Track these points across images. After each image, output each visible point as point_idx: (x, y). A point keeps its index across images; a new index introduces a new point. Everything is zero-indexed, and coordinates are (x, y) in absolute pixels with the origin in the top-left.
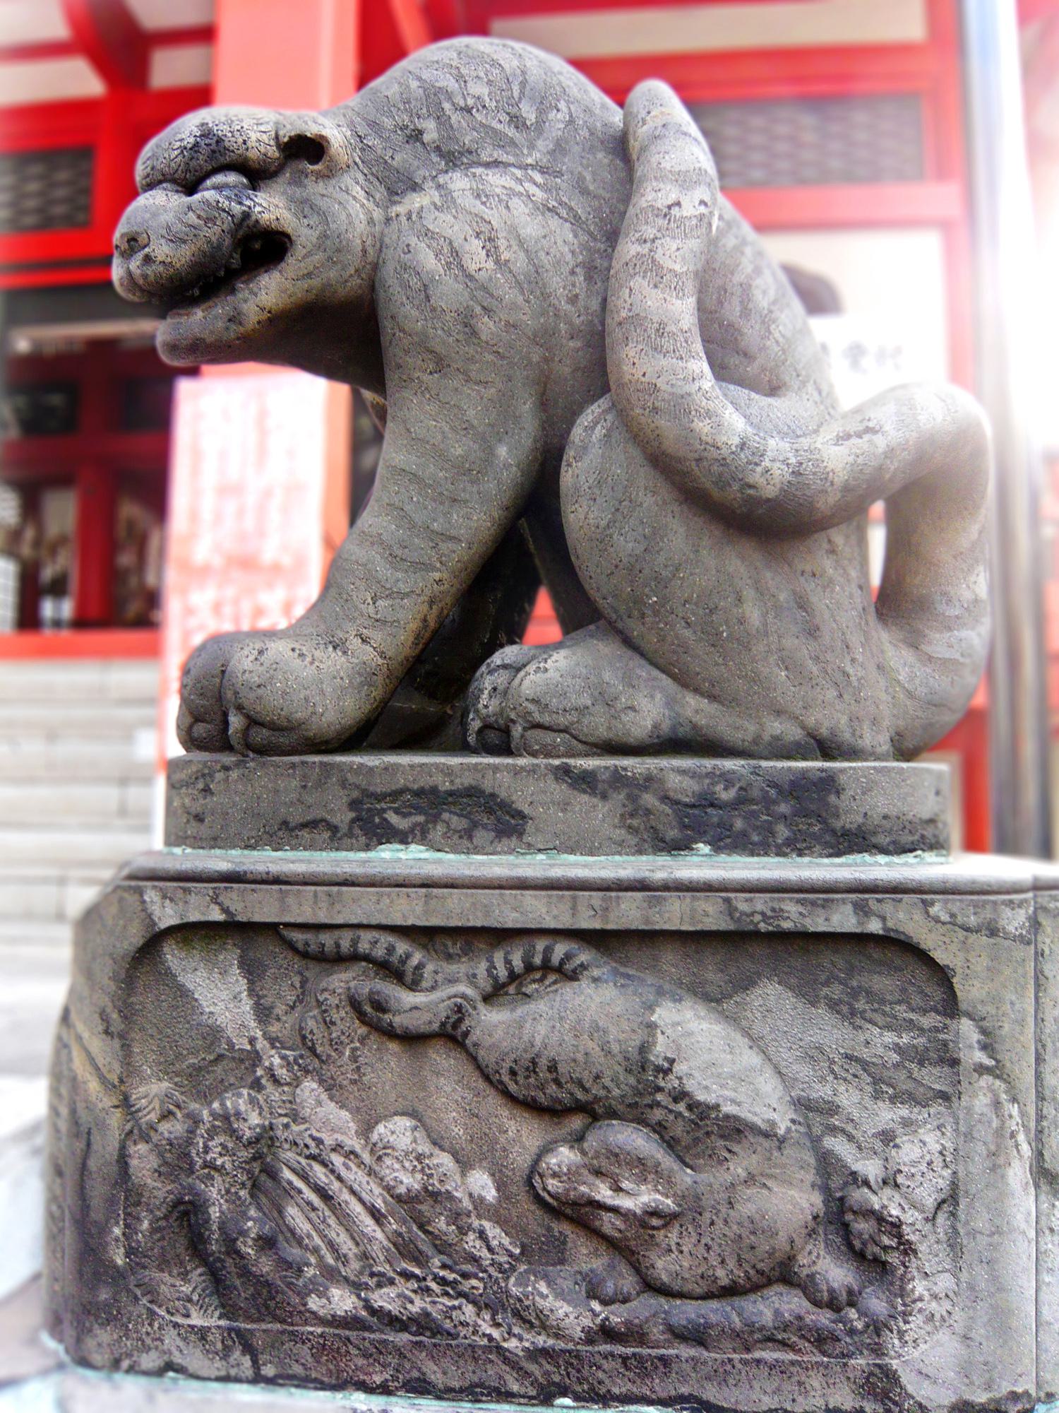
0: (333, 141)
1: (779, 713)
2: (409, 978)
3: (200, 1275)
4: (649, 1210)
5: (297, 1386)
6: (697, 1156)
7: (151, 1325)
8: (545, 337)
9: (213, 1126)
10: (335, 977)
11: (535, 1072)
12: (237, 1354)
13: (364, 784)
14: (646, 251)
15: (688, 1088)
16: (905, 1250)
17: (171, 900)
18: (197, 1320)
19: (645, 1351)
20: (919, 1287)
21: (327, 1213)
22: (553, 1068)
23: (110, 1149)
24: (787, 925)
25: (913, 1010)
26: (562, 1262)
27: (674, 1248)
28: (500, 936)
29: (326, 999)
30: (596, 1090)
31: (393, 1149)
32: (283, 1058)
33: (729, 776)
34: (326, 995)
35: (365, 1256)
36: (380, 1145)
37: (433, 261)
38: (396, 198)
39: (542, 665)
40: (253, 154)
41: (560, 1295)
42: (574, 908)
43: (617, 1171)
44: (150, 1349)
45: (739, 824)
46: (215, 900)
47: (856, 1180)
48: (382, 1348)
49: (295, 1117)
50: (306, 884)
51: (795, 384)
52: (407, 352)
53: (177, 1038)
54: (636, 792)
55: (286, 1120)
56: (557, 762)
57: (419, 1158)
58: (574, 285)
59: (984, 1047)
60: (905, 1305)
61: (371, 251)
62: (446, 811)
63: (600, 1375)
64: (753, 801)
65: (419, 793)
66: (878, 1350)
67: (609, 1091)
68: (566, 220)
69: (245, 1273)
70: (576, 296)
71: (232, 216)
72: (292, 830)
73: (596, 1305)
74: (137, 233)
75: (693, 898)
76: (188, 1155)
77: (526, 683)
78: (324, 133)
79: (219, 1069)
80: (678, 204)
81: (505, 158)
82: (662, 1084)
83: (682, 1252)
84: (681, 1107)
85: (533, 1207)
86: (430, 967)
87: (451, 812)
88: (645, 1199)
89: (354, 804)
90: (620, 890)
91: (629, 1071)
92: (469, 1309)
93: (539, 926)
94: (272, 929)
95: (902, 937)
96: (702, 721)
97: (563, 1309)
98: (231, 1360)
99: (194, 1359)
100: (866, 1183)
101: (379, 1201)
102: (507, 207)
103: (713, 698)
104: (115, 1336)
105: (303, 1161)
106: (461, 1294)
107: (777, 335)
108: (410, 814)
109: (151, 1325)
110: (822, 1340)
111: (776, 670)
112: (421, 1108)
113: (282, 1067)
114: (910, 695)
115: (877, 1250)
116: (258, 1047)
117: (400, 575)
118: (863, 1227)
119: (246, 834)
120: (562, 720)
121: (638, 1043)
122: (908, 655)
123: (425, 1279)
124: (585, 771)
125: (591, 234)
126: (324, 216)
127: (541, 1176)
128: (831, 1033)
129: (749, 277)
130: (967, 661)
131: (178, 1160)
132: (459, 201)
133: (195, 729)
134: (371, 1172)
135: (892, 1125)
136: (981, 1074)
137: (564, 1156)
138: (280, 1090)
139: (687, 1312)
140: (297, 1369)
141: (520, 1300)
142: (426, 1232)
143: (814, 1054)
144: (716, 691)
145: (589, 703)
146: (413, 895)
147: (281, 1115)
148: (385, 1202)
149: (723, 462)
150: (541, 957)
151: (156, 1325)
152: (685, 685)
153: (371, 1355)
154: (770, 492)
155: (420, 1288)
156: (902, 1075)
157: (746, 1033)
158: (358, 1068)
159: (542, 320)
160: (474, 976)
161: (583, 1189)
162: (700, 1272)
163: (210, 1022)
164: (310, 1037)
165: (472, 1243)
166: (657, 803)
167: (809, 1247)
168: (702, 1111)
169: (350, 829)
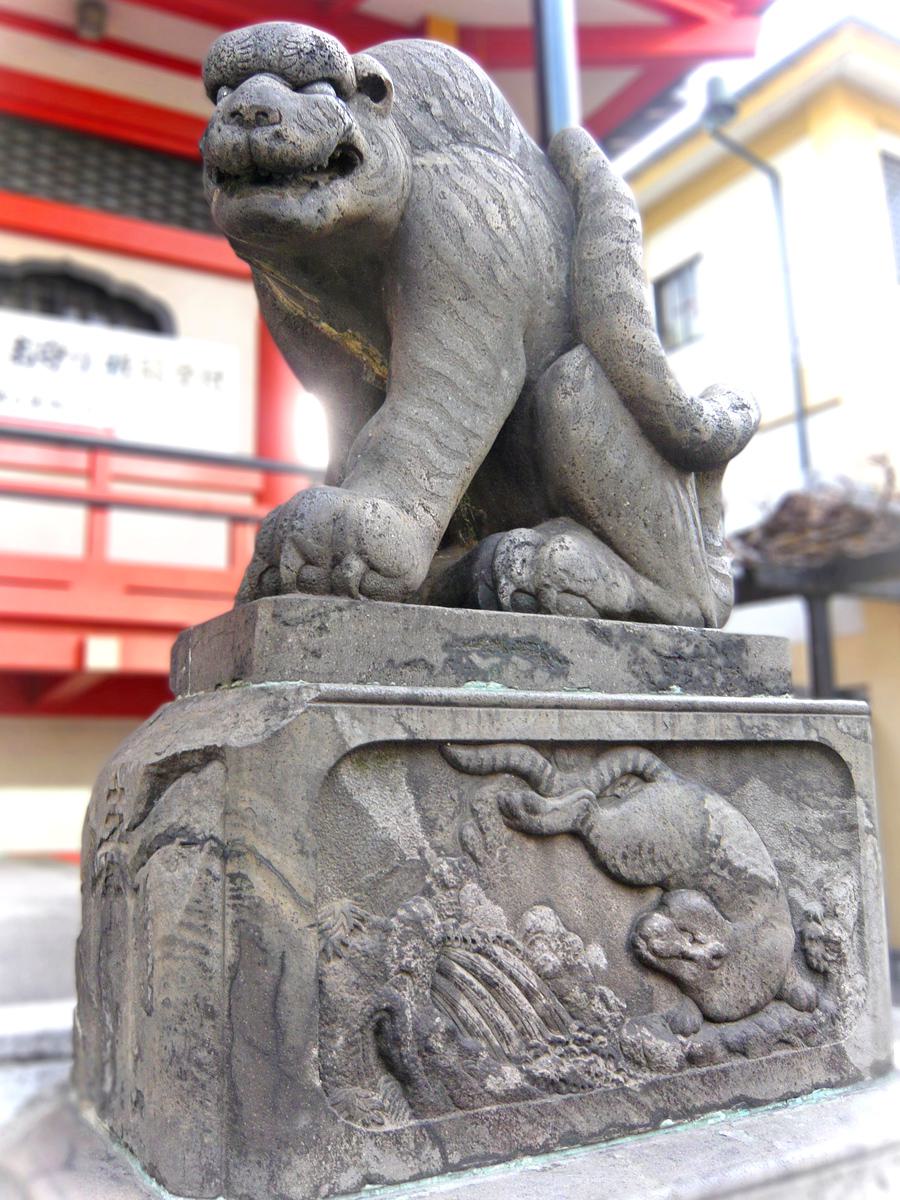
1: (690, 596)
2: (543, 787)
4: (715, 953)
5: (477, 1167)
6: (733, 910)
7: (349, 1141)
9: (406, 932)
10: (485, 788)
11: (640, 854)
14: (624, 248)
17: (359, 721)
18: (389, 1127)
19: (714, 1068)
20: (846, 987)
21: (493, 1000)
22: (651, 851)
23: (307, 970)
24: (771, 736)
26: (651, 1010)
28: (601, 748)
30: (676, 866)
31: (542, 932)
32: (451, 864)
35: (522, 1033)
36: (533, 931)
41: (658, 1035)
42: (654, 724)
43: (695, 926)
45: (696, 672)
46: (398, 720)
47: (809, 917)
48: (542, 1111)
49: (460, 917)
50: (470, 705)
52: (441, 277)
53: (355, 854)
60: (842, 1000)
65: (495, 640)
69: (433, 1069)
73: (682, 1038)
74: (270, 110)
76: (382, 963)
79: (393, 881)
82: (715, 856)
83: (729, 984)
84: (725, 873)
85: (631, 968)
86: (557, 775)
88: (710, 945)
89: (446, 647)
90: (680, 710)
92: (601, 1061)
93: (632, 739)
94: (439, 747)
95: (827, 743)
97: (665, 1045)
98: (423, 1157)
99: (390, 1165)
100: (816, 919)
101: (533, 981)
103: (657, 582)
104: (315, 1162)
105: (472, 956)
106: (595, 1051)
109: (349, 1141)
110: (807, 1034)
112: (552, 897)
113: (449, 872)
115: (826, 964)
118: (816, 949)
119: (358, 670)
120: (584, 588)
123: (567, 1043)
124: (604, 628)
128: (788, 814)
131: (374, 970)
133: (304, 571)
134: (525, 957)
137: (659, 921)
138: (447, 893)
139: (733, 1032)
140: (479, 1150)
141: (634, 1045)
143: (781, 830)
147: (449, 916)
148: (537, 980)
149: (682, 410)
151: (354, 1140)
152: (638, 571)
154: (706, 437)
156: (823, 840)
161: (677, 943)
163: (384, 836)
165: (597, 1006)
166: (649, 654)
169: (444, 669)
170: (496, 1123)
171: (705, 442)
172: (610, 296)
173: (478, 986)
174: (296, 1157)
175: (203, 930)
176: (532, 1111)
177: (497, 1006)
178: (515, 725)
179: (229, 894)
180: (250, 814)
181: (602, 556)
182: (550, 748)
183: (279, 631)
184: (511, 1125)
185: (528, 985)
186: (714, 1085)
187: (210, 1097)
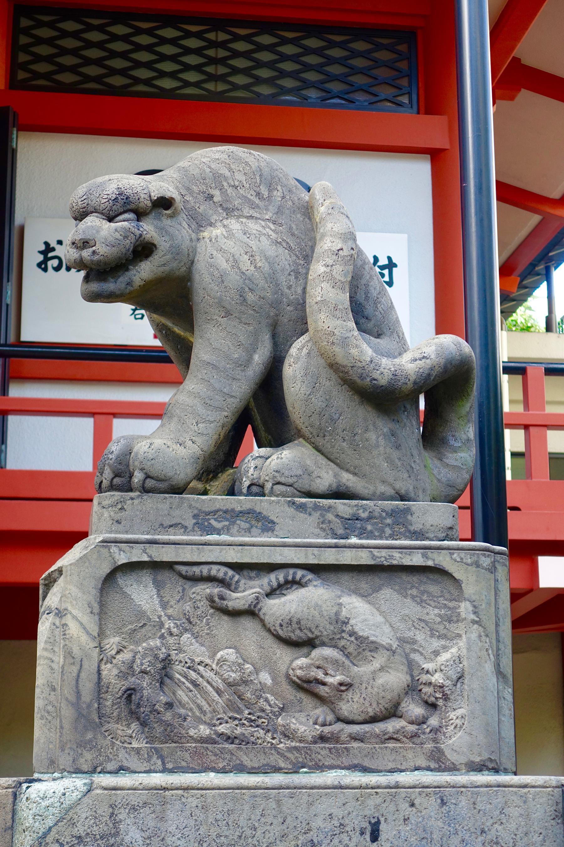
0: (176, 200)
2: (233, 587)
3: (135, 725)
6: (359, 660)
8: (276, 304)
11: (291, 624)
12: (155, 758)
13: (200, 508)
15: (356, 630)
16: (445, 698)
17: (124, 551)
18: (135, 745)
21: (196, 692)
22: (299, 622)
24: (395, 562)
25: (446, 600)
27: (350, 700)
29: (195, 597)
33: (365, 507)
34: (194, 595)
37: (225, 264)
38: (202, 229)
39: (280, 456)
40: (141, 205)
44: (111, 760)
45: (369, 527)
46: (144, 551)
48: (222, 751)
49: (180, 650)
51: (388, 333)
54: (325, 513)
55: (176, 652)
56: (289, 499)
57: (239, 665)
58: (290, 281)
59: (475, 613)
61: (191, 254)
62: (239, 520)
63: (319, 757)
64: (375, 518)
65: (226, 512)
66: (435, 741)
67: (322, 633)
68: (286, 249)
70: (291, 286)
71: (136, 236)
72: (165, 528)
74: (90, 240)
75: (356, 551)
77: (273, 463)
78: (173, 196)
79: (143, 630)
80: (342, 249)
81: (255, 215)
82: (345, 629)
83: (353, 701)
84: (353, 639)
85: (288, 687)
87: (241, 520)
89: (195, 516)
90: (326, 547)
91: (331, 623)
94: (170, 566)
95: (442, 568)
96: (350, 484)
98: (152, 762)
101: (221, 686)
102: (259, 241)
103: (355, 474)
104: (94, 756)
105: (185, 669)
107: (381, 309)
108: (222, 521)
111: (383, 463)
114: (439, 480)
116: (162, 619)
117: (209, 413)
121: (334, 611)
122: (437, 462)
124: (302, 503)
125: (297, 256)
126: (172, 237)
127: (293, 670)
129: (368, 281)
130: (465, 467)
132: (236, 235)
133: (115, 480)
135: (438, 648)
136: (474, 624)
140: (184, 764)
141: (284, 726)
142: (242, 699)
144: (356, 471)
145: (302, 474)
146: (236, 549)
147: (174, 650)
148: (223, 686)
150: (291, 576)
151: (115, 748)
152: (342, 468)
153: (218, 755)
154: (383, 381)
155: (239, 723)
156: (442, 627)
157: (378, 609)
158: (210, 628)
159: (276, 296)
160: (262, 585)
162: (361, 710)
163: (139, 609)
164: (188, 614)
166: (334, 518)
167: (406, 699)
168: (361, 640)
169: (193, 528)
170: (194, 753)
171: (382, 386)
172: (317, 303)
173: (188, 684)
174: (85, 752)
175: (52, 651)
176: (216, 750)
177: (198, 696)
179: (62, 634)
180: (69, 595)
182: (238, 567)
183: (101, 511)
184: (203, 754)
185: (218, 688)
186: (339, 755)
187: (52, 726)
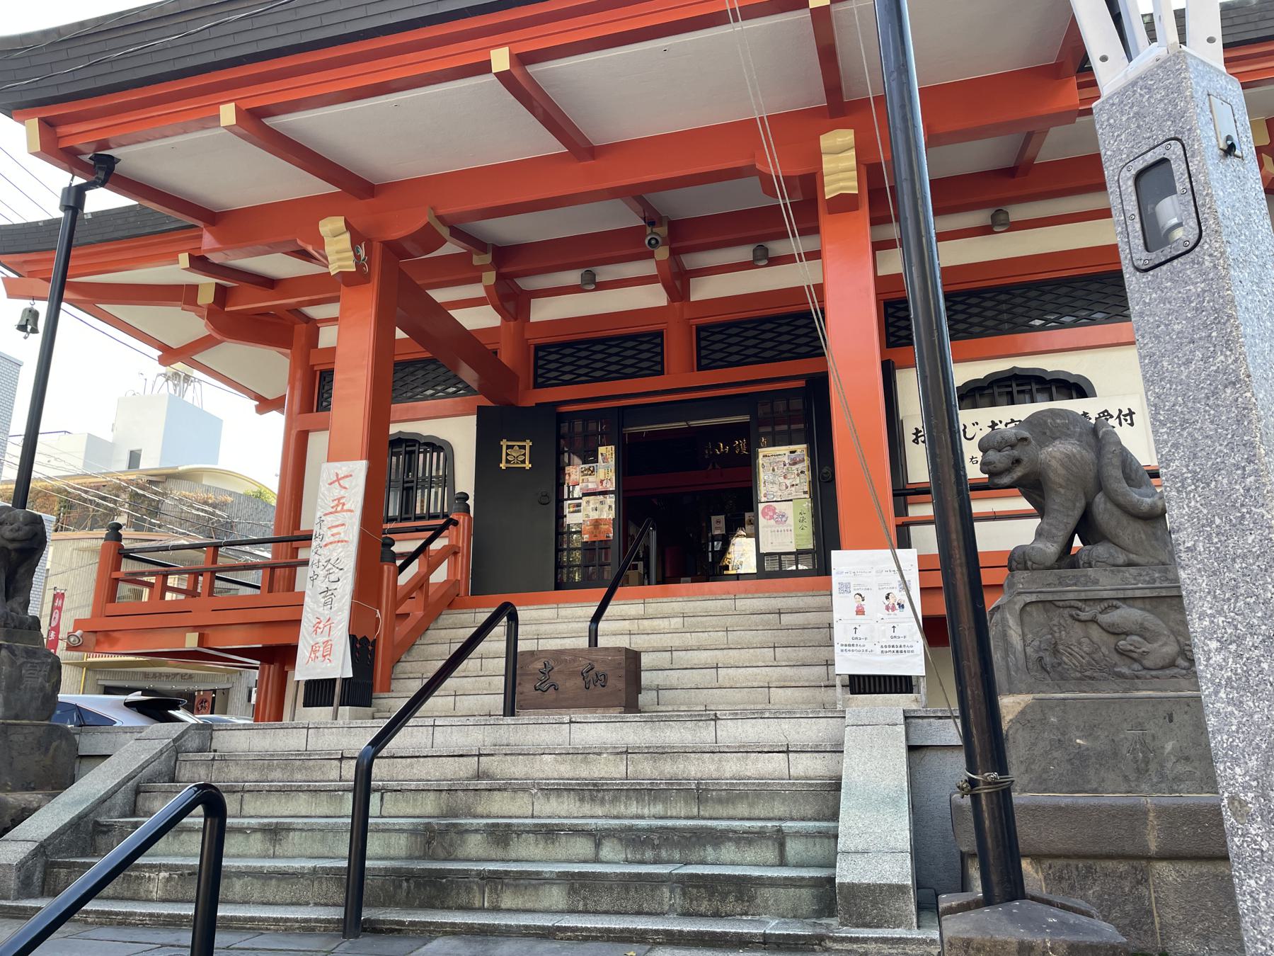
178: (1071, 596)
181: (1113, 549)
